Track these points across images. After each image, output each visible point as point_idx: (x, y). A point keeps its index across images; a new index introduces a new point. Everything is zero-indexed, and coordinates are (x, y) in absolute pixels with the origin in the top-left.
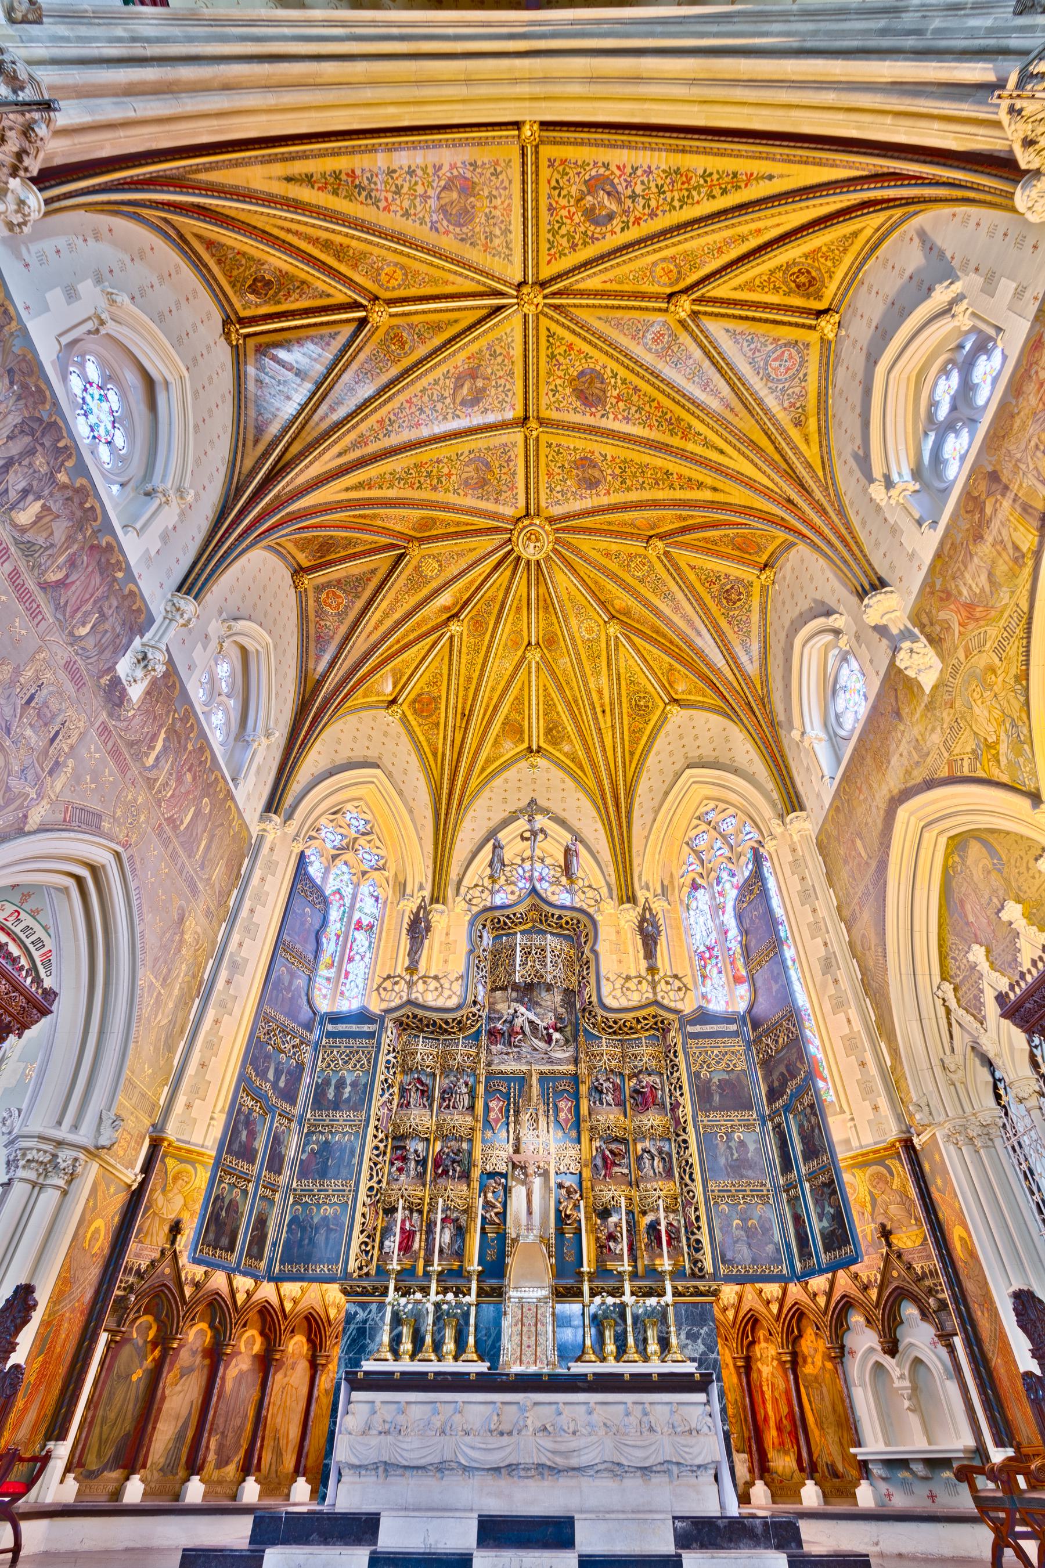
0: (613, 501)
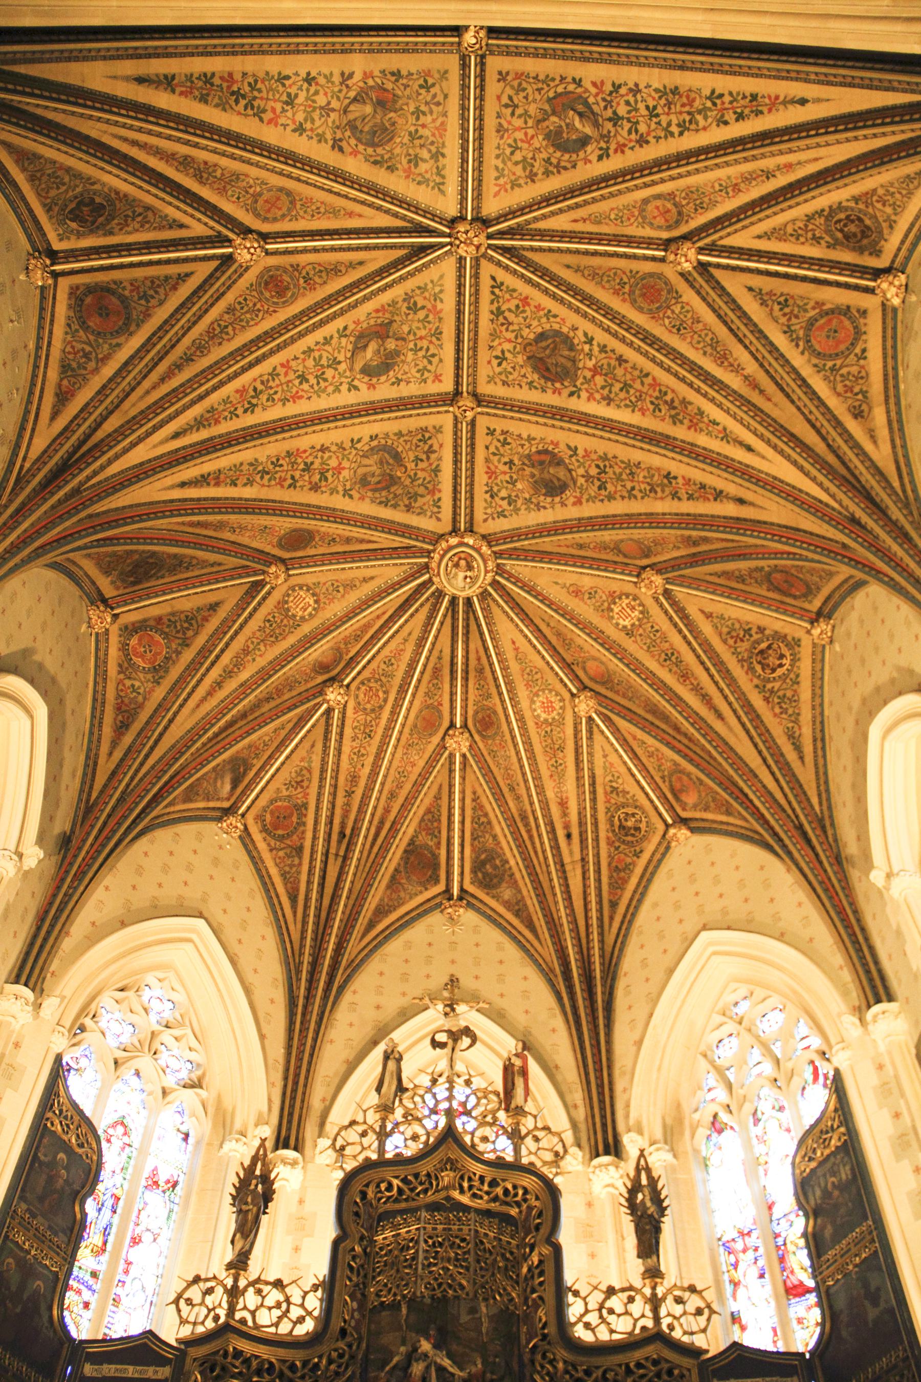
0: (587, 514)
